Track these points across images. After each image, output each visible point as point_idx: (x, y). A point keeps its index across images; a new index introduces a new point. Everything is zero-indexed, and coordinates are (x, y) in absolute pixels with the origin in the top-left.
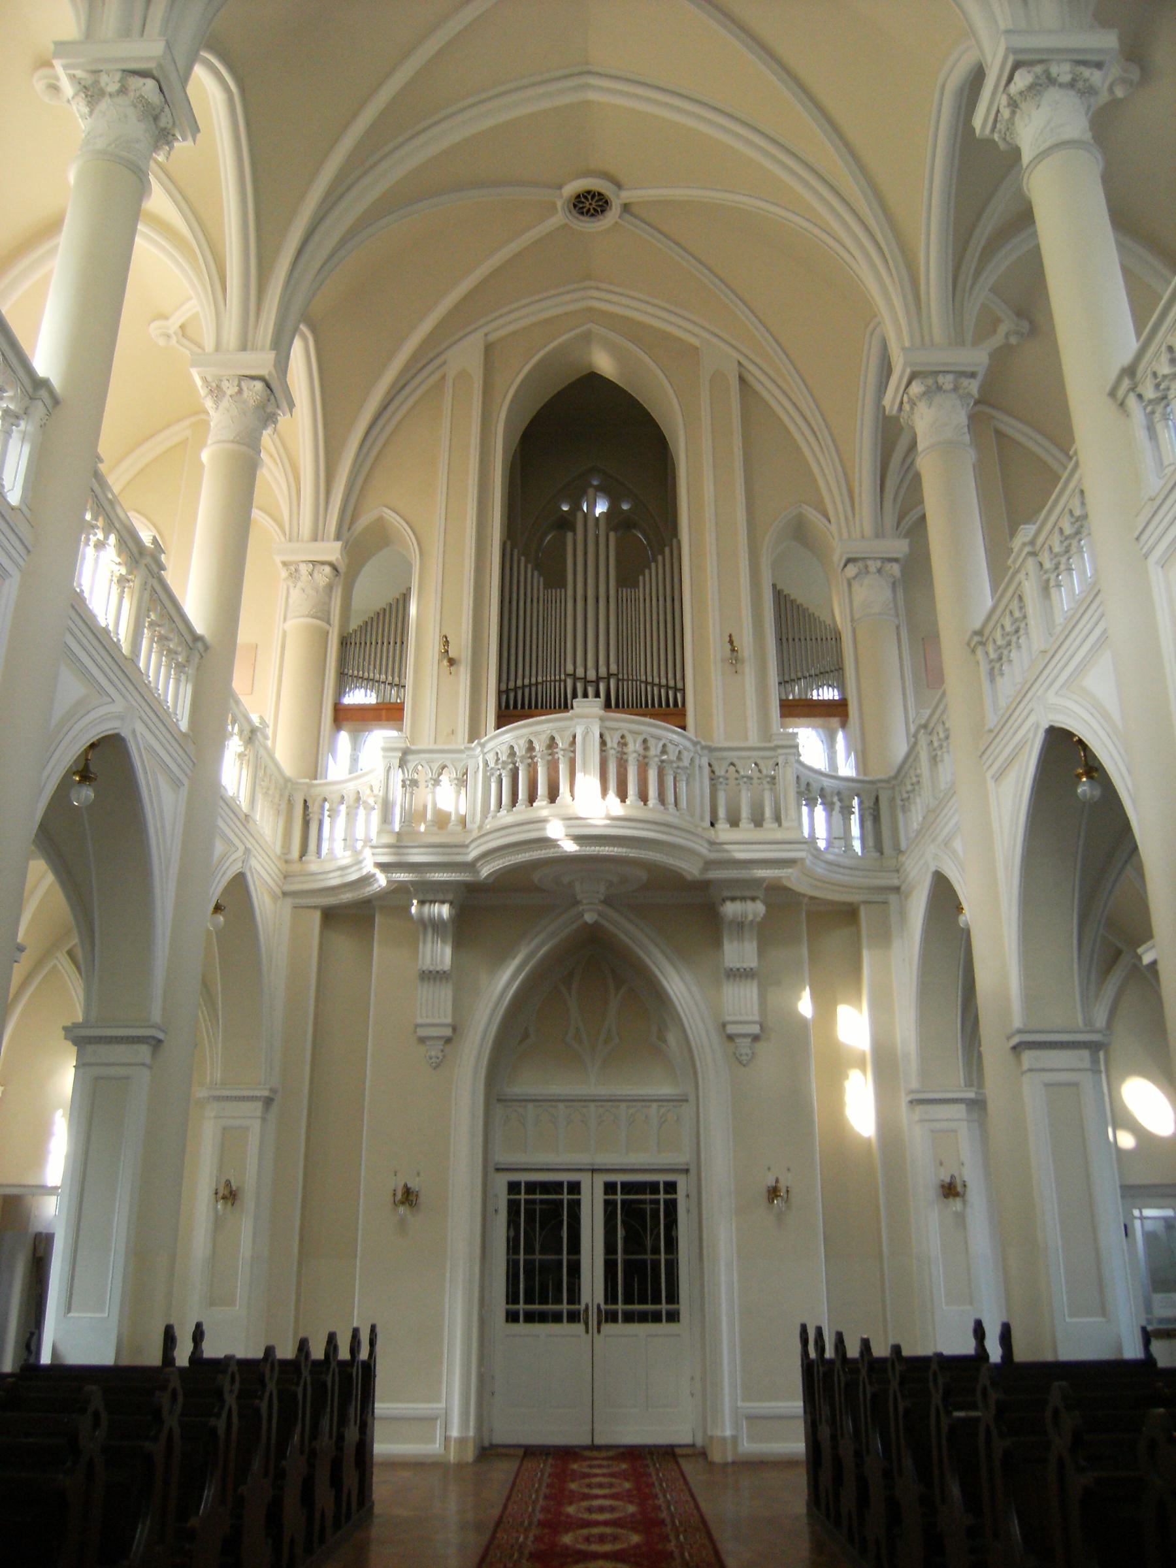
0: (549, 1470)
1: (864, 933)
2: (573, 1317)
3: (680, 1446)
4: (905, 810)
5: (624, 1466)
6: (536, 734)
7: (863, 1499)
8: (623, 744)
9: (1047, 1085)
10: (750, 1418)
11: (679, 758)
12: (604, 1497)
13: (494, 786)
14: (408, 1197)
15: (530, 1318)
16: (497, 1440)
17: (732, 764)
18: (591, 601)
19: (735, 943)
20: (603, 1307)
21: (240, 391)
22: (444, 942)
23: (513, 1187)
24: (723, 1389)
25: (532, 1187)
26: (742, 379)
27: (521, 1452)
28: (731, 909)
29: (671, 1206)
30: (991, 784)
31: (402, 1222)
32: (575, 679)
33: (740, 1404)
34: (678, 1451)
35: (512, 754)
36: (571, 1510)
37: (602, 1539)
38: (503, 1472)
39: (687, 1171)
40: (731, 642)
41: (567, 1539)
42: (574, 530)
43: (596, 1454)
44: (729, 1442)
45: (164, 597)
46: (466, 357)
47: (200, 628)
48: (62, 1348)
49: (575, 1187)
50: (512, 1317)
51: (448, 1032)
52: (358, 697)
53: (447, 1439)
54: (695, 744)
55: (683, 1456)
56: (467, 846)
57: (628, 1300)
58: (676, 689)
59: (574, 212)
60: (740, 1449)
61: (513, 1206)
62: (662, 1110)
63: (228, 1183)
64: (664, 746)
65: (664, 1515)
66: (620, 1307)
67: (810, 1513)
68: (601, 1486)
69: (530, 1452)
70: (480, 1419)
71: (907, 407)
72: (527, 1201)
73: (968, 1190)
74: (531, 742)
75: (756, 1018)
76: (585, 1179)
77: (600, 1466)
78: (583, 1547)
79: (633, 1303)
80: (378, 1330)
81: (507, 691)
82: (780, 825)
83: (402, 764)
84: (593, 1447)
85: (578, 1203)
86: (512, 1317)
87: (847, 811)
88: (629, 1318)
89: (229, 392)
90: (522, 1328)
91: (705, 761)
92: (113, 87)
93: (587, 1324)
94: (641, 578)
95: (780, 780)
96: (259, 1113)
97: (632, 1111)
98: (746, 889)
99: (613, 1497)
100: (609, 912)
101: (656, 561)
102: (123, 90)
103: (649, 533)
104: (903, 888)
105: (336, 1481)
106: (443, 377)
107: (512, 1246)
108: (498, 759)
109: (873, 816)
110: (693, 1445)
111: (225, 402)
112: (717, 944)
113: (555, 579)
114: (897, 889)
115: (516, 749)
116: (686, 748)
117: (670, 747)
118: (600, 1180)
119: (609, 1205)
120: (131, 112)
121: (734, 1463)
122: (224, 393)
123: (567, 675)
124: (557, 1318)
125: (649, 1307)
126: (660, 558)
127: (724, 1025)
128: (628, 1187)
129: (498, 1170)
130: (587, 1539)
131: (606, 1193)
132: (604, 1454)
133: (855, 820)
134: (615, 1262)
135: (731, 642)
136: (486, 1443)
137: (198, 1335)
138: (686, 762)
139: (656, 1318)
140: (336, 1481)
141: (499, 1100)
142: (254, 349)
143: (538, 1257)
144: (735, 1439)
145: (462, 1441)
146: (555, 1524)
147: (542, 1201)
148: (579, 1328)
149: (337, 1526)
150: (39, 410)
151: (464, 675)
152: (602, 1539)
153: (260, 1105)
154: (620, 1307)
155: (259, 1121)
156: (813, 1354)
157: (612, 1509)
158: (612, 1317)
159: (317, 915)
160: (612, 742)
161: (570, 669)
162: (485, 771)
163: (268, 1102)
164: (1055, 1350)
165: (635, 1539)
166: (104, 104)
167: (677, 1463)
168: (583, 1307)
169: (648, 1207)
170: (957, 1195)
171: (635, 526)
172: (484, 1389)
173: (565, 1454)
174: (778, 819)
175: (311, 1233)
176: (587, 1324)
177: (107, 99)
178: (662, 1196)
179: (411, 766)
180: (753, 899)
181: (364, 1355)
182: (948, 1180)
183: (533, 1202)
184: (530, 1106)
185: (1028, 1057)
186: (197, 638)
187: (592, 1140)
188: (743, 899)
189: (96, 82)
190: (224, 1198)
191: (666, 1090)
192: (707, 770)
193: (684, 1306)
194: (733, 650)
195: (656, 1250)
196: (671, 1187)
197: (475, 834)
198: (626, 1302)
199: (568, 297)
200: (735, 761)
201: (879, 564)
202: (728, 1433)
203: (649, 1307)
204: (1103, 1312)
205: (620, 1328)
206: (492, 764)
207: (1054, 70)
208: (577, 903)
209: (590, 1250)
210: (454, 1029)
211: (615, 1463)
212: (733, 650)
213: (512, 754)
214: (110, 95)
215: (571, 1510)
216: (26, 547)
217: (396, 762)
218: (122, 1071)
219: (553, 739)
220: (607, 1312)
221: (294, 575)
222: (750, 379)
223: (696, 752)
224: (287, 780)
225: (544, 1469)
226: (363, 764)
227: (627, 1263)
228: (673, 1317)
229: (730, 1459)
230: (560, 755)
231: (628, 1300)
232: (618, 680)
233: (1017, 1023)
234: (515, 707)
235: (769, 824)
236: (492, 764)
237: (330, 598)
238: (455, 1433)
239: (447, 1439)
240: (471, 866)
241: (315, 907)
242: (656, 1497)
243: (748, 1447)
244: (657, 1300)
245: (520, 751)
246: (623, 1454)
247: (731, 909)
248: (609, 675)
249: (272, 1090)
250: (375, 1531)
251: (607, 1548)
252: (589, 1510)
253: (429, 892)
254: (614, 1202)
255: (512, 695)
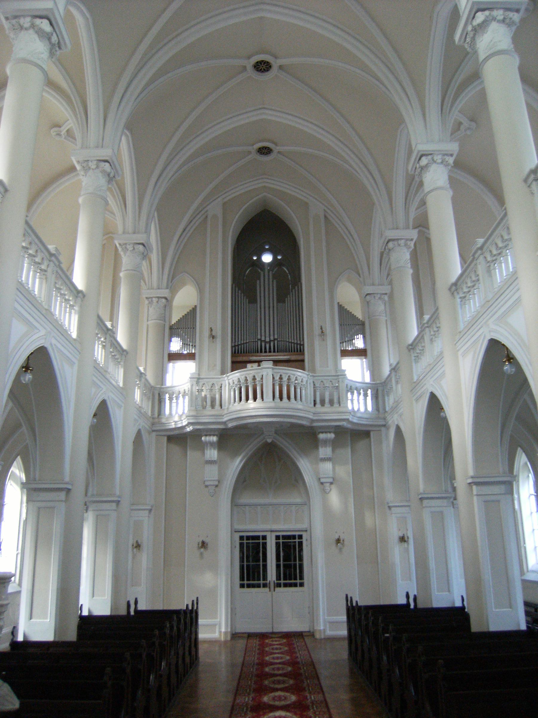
0: (258, 642)
1: (372, 440)
2: (265, 586)
3: (305, 632)
4: (388, 396)
5: (285, 641)
6: (248, 374)
7: (363, 656)
8: (281, 378)
9: (431, 512)
10: (330, 623)
11: (302, 381)
12: (277, 645)
13: (232, 393)
14: (204, 545)
15: (249, 586)
16: (238, 631)
17: (322, 381)
18: (267, 309)
19: (324, 448)
20: (276, 582)
21: (134, 249)
22: (214, 449)
23: (241, 538)
24: (319, 611)
25: (248, 538)
26: (325, 217)
27: (246, 635)
28: (321, 436)
29: (301, 544)
30: (414, 402)
31: (201, 554)
32: (261, 341)
33: (326, 618)
34: (304, 634)
35: (239, 381)
36: (267, 658)
37: (278, 669)
38: (241, 644)
39: (306, 531)
40: (321, 328)
41: (267, 669)
42: (259, 279)
43: (274, 636)
44: (322, 631)
45: (116, 344)
46: (215, 209)
47: (125, 346)
48: (92, 609)
49: (264, 538)
50: (242, 586)
51: (217, 483)
52: (176, 345)
53: (220, 632)
54: (308, 375)
55: (305, 636)
56: (223, 416)
57: (285, 579)
58: (300, 345)
59: (258, 154)
60: (326, 634)
61: (241, 545)
62: (297, 508)
63: (137, 542)
64: (296, 377)
65: (299, 660)
66: (282, 581)
67: (349, 659)
68: (277, 649)
69: (250, 636)
70: (232, 625)
71: (387, 250)
72: (246, 543)
73: (409, 539)
74: (246, 377)
75: (332, 476)
76: (268, 535)
77: (276, 641)
78: (272, 672)
79: (287, 580)
80: (199, 599)
81: (235, 346)
82: (340, 405)
83: (197, 383)
84: (273, 633)
85: (266, 543)
86: (242, 586)
87: (366, 395)
88: (286, 585)
89: (130, 249)
90: (246, 590)
91: (312, 381)
92: (94, 167)
93: (270, 588)
94: (286, 299)
95: (341, 388)
96: (147, 515)
97: (285, 508)
98: (326, 430)
99: (280, 644)
100: (278, 437)
101: (292, 291)
102: (97, 167)
103: (288, 279)
104: (387, 425)
105: (190, 653)
106: (207, 217)
107: (242, 560)
108: (234, 383)
109: (376, 397)
110: (309, 632)
111: (128, 253)
112: (316, 447)
113: (253, 300)
114: (384, 426)
115: (241, 380)
116: (304, 377)
117: (299, 378)
118: (274, 534)
119: (278, 544)
120: (100, 175)
121: (324, 639)
122: (128, 250)
123: (258, 339)
124: (258, 586)
125: (293, 581)
126: (294, 291)
127: (319, 479)
128: (284, 537)
129: (235, 532)
130: (273, 669)
131: (276, 539)
132: (277, 636)
133: (369, 399)
134: (280, 565)
135: (321, 328)
136: (234, 633)
137: (136, 602)
138: (304, 383)
139: (295, 585)
140: (190, 653)
141: (235, 505)
142: (138, 233)
143: (251, 563)
144: (324, 630)
145: (226, 633)
146: (262, 664)
147: (252, 543)
148: (267, 589)
149: (191, 667)
150: (79, 300)
151: (219, 341)
152: (278, 669)
153: (147, 512)
154: (282, 581)
155: (147, 518)
156: (349, 604)
157: (281, 658)
158: (279, 585)
159: (166, 438)
160: (277, 378)
161: (259, 337)
162: (229, 387)
163: (150, 510)
164: (432, 604)
165: (290, 669)
166: (90, 172)
167: (304, 639)
168: (268, 582)
169: (292, 544)
170: (405, 541)
171: (284, 265)
172: (233, 612)
173: (263, 636)
174: (339, 403)
175: (169, 561)
176: (270, 588)
177: (91, 171)
178: (297, 540)
179: (201, 384)
180: (330, 432)
181: (195, 608)
182: (402, 535)
183: (249, 543)
184: (247, 507)
185: (425, 502)
186: (124, 351)
187: (271, 521)
188: (326, 432)
189: (88, 165)
190: (136, 547)
191: (298, 500)
192: (312, 384)
193: (306, 580)
194: (322, 332)
195: (295, 560)
196: (300, 537)
197: (226, 412)
198: (284, 580)
199: (256, 182)
200: (324, 381)
201: (379, 296)
202: (322, 628)
203: (293, 581)
204: (449, 591)
205: (282, 589)
206: (231, 384)
207: (435, 158)
208: (263, 433)
209: (270, 561)
210: (219, 482)
211: (281, 639)
212: (322, 332)
213: (239, 381)
214: (93, 169)
215: (267, 658)
216: (78, 351)
217: (195, 383)
218: (107, 513)
219: (254, 376)
220: (277, 583)
221: (151, 303)
222: (329, 217)
223: (308, 378)
224: (152, 387)
225: (255, 642)
226: (180, 375)
227: (284, 565)
228: (302, 585)
229: (323, 637)
230: (257, 383)
231: (285, 579)
232: (278, 341)
233: (421, 491)
234: (238, 353)
235: (336, 405)
236: (231, 384)
237: (165, 311)
238: (223, 630)
239: (220, 632)
240: (225, 423)
241: (164, 435)
242: (296, 653)
243: (329, 633)
244: (295, 579)
245: (242, 381)
246: (284, 635)
247: (321, 436)
248: (275, 339)
249: (152, 506)
250: (200, 668)
251: (280, 672)
252: (273, 658)
253: (209, 432)
254: (279, 543)
255: (237, 348)
